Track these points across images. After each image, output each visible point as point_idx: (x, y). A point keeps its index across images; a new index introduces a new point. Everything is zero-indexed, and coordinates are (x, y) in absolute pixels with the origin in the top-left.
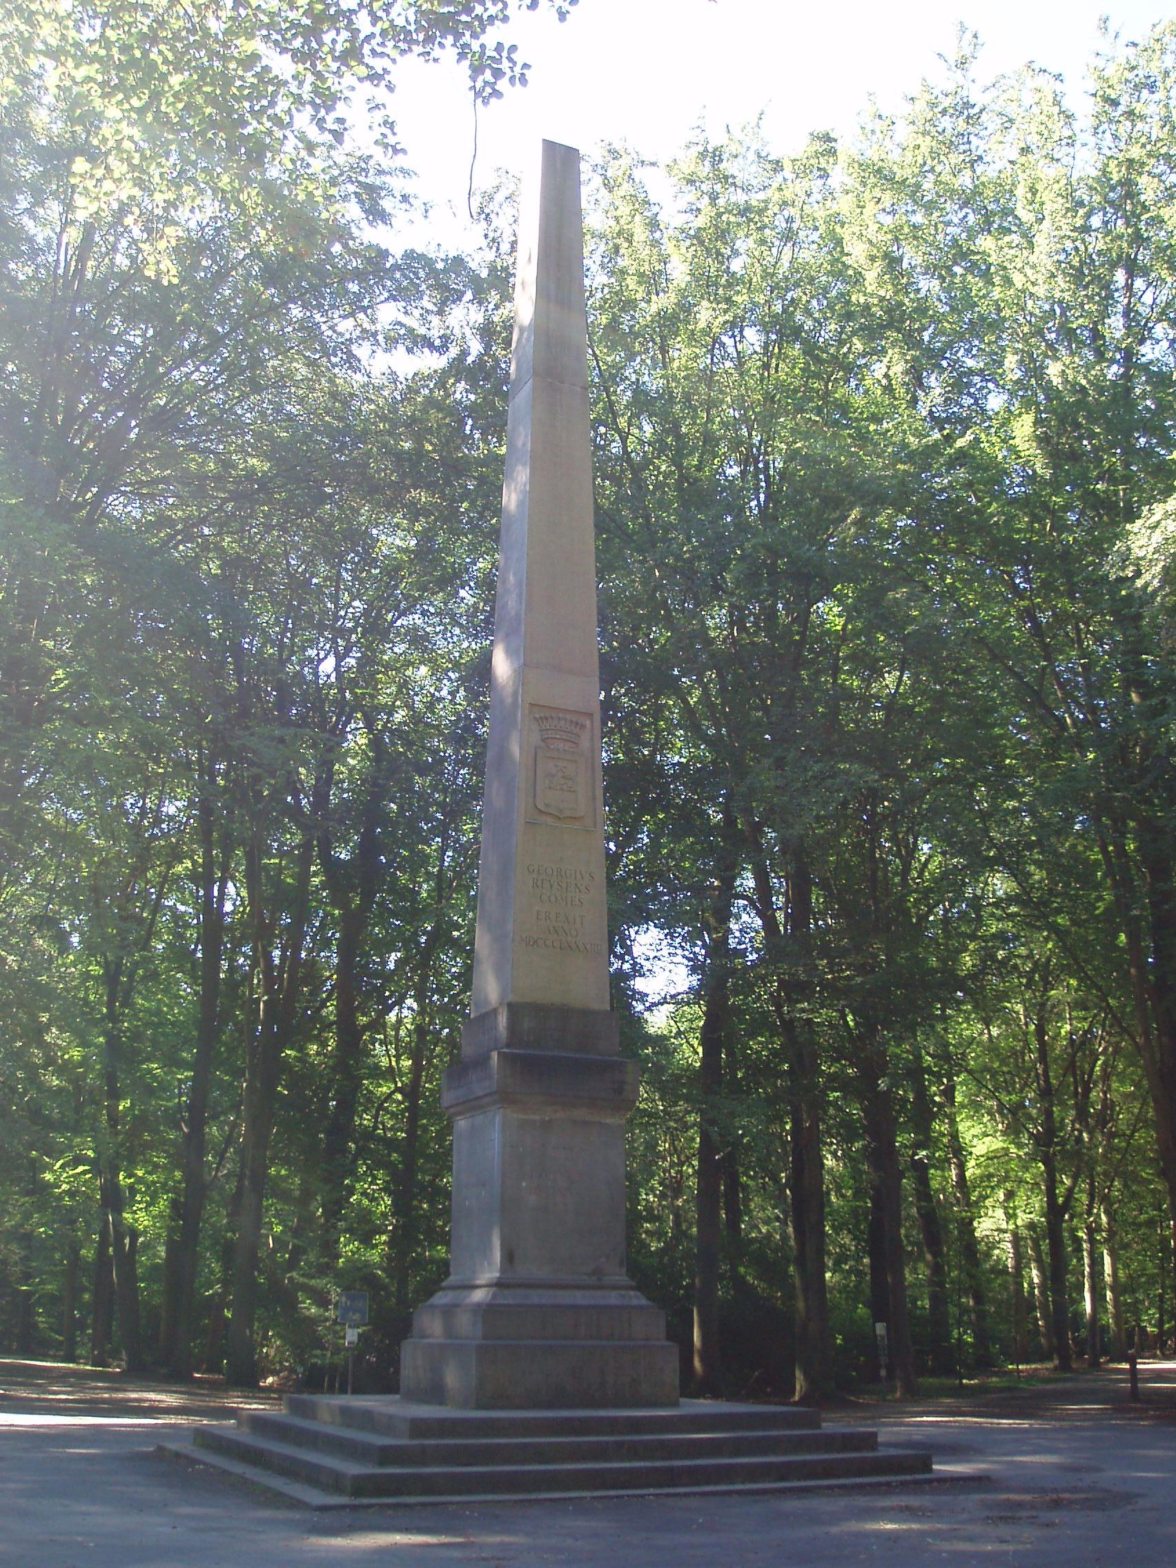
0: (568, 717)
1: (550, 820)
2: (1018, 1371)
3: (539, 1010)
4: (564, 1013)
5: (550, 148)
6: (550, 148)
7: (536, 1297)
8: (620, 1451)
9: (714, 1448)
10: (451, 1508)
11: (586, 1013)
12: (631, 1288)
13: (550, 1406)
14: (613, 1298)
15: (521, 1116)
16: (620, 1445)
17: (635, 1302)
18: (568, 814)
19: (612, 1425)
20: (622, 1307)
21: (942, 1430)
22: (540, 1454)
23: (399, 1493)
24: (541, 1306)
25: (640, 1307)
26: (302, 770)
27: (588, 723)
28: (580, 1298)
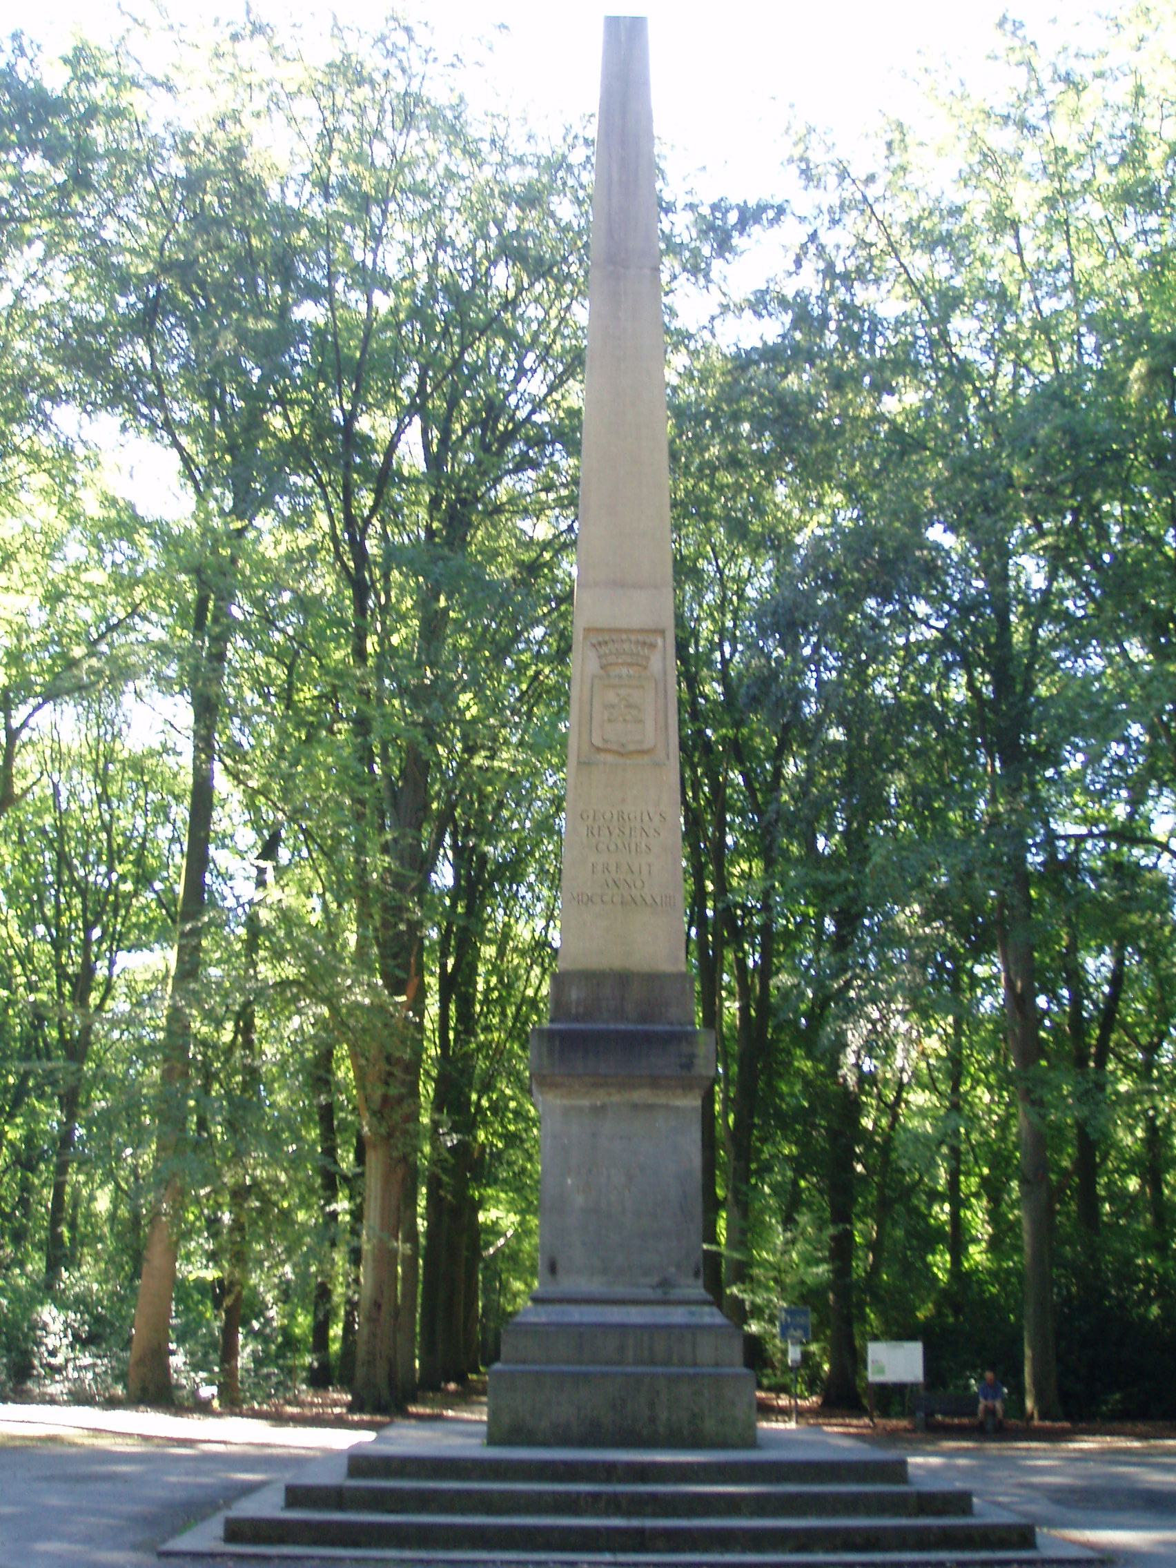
0: (633, 638)
1: (610, 758)
2: (498, 1249)
3: (592, 978)
4: (623, 979)
5: (613, 23)
6: (613, 23)
7: (577, 1314)
8: (593, 1504)
9: (760, 1506)
10: (308, 1564)
11: (652, 978)
12: (705, 1303)
13: (583, 1443)
14: (678, 1315)
15: (566, 1102)
16: (596, 1496)
17: (707, 1320)
18: (631, 747)
19: (609, 1471)
20: (687, 1327)
21: (74, 1450)
22: (486, 1503)
23: (282, 1541)
24: (580, 1325)
25: (709, 1328)
26: (750, 963)
27: (660, 642)
28: (635, 1315)
